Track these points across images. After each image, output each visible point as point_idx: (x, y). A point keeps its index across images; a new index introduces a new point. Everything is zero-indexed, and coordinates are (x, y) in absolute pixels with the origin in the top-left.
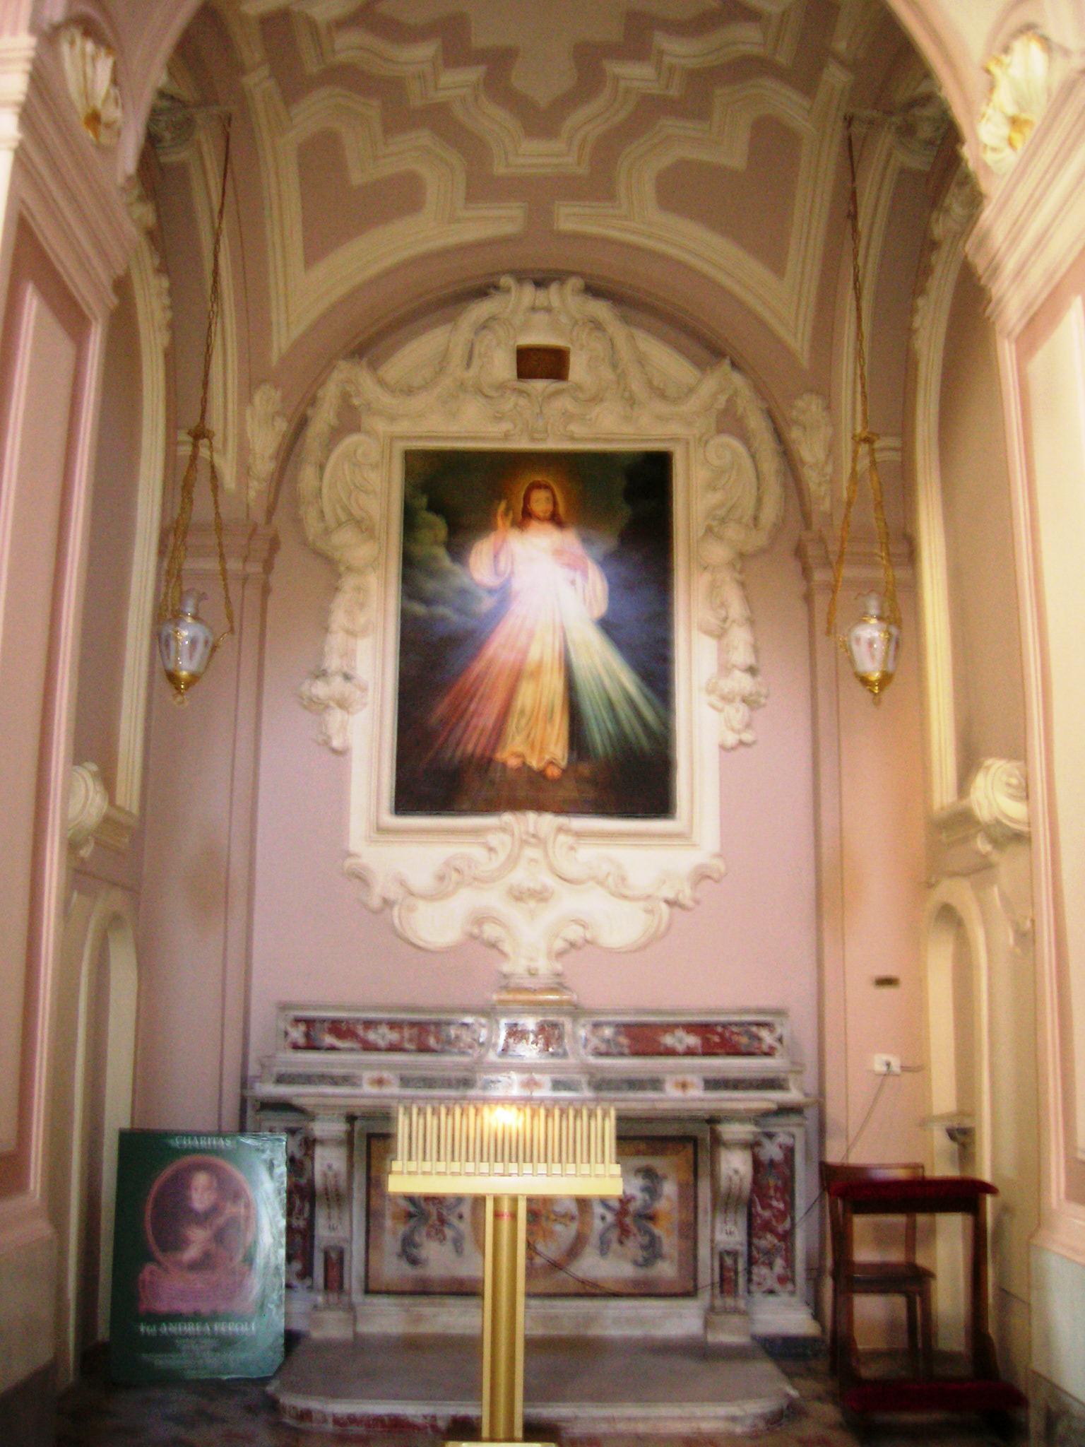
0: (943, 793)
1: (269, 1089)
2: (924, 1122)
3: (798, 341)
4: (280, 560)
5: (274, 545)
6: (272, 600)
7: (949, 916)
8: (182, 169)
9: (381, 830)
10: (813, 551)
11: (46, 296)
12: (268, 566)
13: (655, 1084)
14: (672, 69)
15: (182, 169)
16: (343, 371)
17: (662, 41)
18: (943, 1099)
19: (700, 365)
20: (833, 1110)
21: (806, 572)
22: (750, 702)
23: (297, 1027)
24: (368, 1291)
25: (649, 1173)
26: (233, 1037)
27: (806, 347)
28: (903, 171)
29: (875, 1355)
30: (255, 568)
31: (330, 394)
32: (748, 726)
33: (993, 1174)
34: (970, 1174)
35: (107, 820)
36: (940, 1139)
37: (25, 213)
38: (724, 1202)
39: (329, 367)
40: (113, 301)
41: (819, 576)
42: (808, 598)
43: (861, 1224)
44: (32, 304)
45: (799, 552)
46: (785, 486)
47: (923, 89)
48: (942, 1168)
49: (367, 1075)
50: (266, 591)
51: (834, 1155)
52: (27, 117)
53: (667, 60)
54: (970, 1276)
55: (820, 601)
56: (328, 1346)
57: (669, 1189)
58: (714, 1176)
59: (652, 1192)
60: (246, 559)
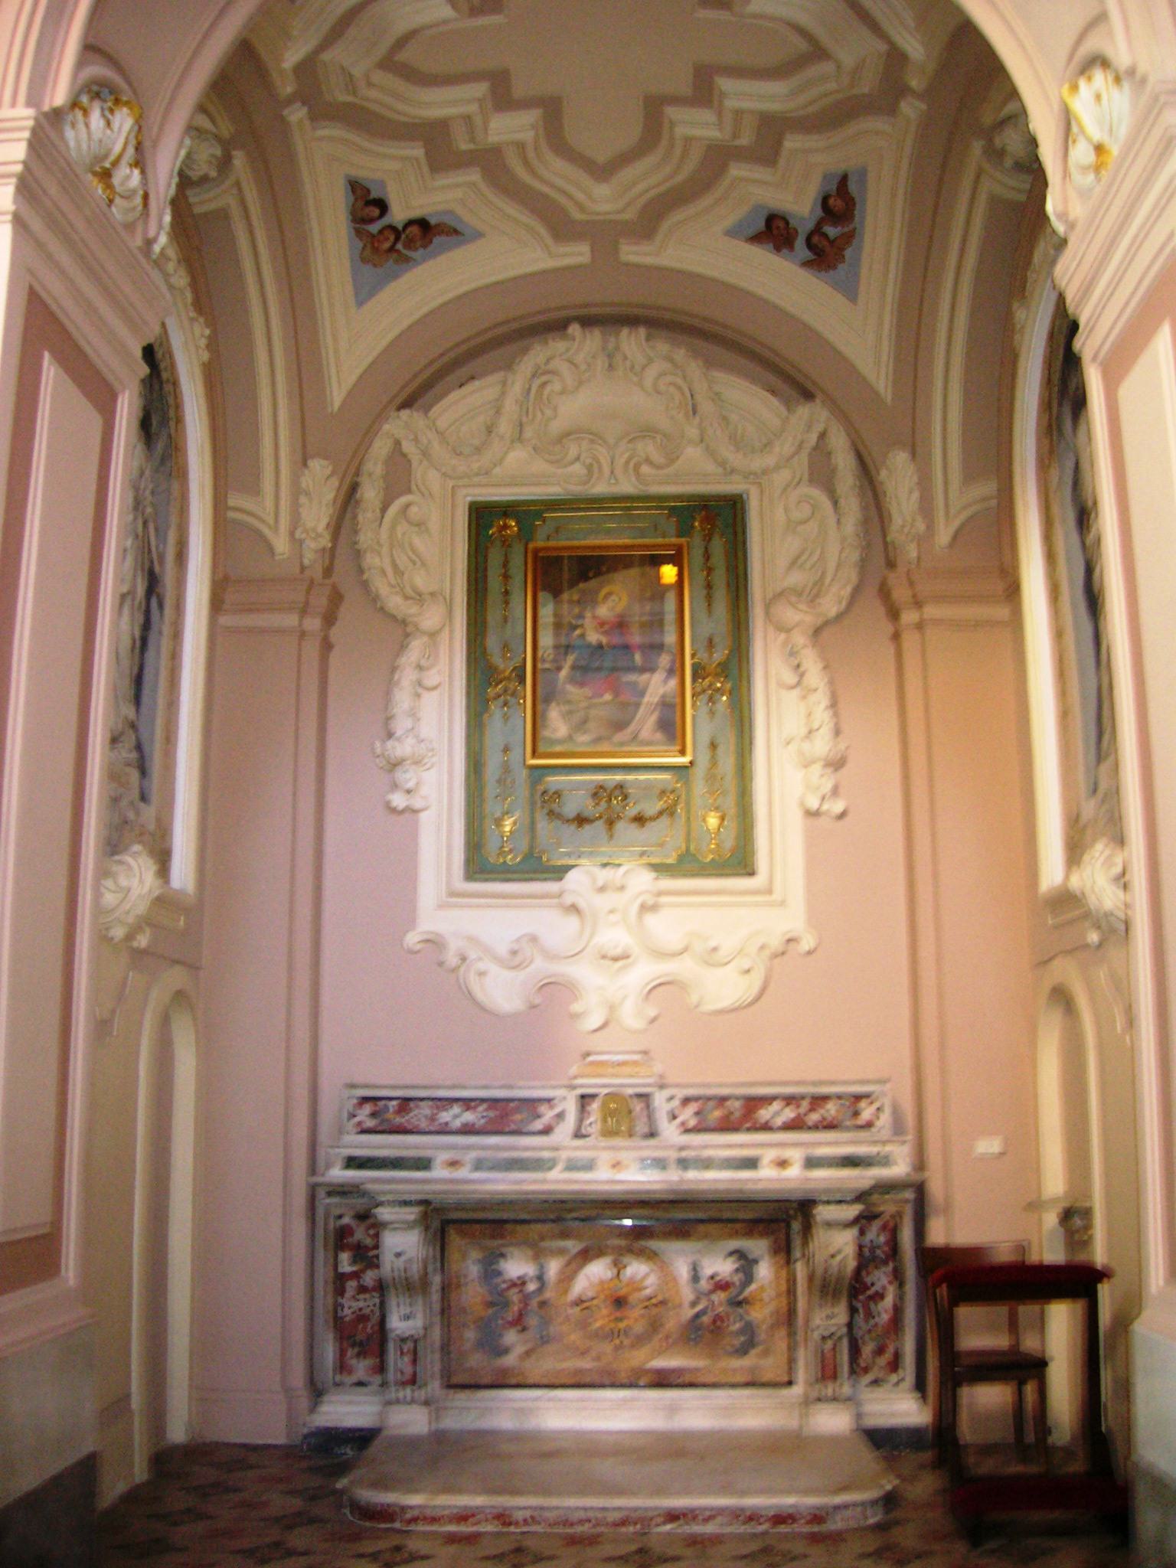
0: (1052, 871)
1: (338, 1174)
2: (1035, 1206)
3: (881, 380)
4: (344, 612)
5: (336, 598)
6: (334, 658)
7: (1062, 997)
8: (223, 215)
9: (453, 894)
10: (901, 593)
11: (61, 359)
12: (329, 619)
13: (423, 1164)
14: (738, 113)
15: (223, 215)
16: (399, 425)
17: (724, 84)
18: (1055, 1183)
19: (788, 404)
20: (936, 1189)
21: (894, 614)
22: (836, 764)
23: (547, 343)
24: (451, 1386)
25: (739, 1254)
26: (301, 1117)
27: (890, 390)
28: (994, 201)
29: (987, 1450)
30: (313, 624)
31: (380, 448)
32: (835, 791)
33: (1110, 1249)
34: (1081, 1257)
35: (160, 901)
36: (1051, 1219)
37: (37, 288)
38: (826, 1288)
39: (380, 418)
40: (144, 370)
41: (909, 617)
42: (896, 637)
43: (966, 1314)
44: (50, 371)
45: (884, 593)
46: (865, 508)
47: (1011, 108)
48: (1051, 1252)
49: (442, 1157)
50: (327, 646)
51: (938, 1235)
52: (26, 187)
53: (731, 103)
54: (1080, 1327)
55: (910, 640)
56: (412, 1443)
57: (765, 1271)
58: (807, 1259)
59: (749, 1278)
60: (304, 612)
